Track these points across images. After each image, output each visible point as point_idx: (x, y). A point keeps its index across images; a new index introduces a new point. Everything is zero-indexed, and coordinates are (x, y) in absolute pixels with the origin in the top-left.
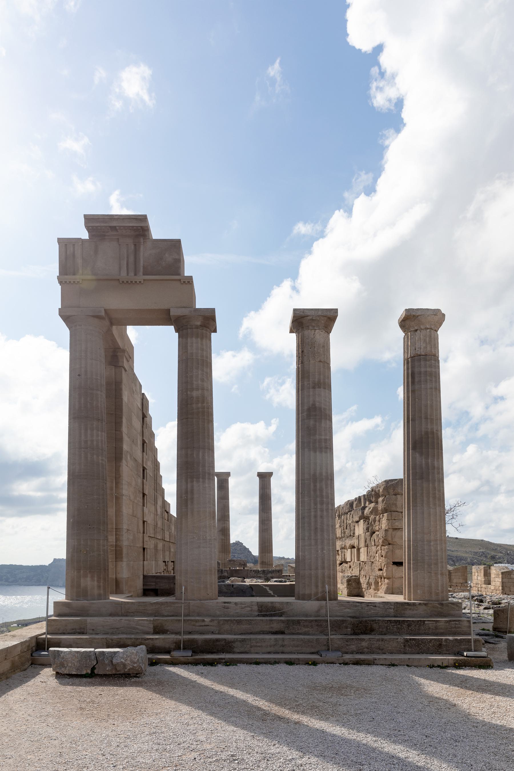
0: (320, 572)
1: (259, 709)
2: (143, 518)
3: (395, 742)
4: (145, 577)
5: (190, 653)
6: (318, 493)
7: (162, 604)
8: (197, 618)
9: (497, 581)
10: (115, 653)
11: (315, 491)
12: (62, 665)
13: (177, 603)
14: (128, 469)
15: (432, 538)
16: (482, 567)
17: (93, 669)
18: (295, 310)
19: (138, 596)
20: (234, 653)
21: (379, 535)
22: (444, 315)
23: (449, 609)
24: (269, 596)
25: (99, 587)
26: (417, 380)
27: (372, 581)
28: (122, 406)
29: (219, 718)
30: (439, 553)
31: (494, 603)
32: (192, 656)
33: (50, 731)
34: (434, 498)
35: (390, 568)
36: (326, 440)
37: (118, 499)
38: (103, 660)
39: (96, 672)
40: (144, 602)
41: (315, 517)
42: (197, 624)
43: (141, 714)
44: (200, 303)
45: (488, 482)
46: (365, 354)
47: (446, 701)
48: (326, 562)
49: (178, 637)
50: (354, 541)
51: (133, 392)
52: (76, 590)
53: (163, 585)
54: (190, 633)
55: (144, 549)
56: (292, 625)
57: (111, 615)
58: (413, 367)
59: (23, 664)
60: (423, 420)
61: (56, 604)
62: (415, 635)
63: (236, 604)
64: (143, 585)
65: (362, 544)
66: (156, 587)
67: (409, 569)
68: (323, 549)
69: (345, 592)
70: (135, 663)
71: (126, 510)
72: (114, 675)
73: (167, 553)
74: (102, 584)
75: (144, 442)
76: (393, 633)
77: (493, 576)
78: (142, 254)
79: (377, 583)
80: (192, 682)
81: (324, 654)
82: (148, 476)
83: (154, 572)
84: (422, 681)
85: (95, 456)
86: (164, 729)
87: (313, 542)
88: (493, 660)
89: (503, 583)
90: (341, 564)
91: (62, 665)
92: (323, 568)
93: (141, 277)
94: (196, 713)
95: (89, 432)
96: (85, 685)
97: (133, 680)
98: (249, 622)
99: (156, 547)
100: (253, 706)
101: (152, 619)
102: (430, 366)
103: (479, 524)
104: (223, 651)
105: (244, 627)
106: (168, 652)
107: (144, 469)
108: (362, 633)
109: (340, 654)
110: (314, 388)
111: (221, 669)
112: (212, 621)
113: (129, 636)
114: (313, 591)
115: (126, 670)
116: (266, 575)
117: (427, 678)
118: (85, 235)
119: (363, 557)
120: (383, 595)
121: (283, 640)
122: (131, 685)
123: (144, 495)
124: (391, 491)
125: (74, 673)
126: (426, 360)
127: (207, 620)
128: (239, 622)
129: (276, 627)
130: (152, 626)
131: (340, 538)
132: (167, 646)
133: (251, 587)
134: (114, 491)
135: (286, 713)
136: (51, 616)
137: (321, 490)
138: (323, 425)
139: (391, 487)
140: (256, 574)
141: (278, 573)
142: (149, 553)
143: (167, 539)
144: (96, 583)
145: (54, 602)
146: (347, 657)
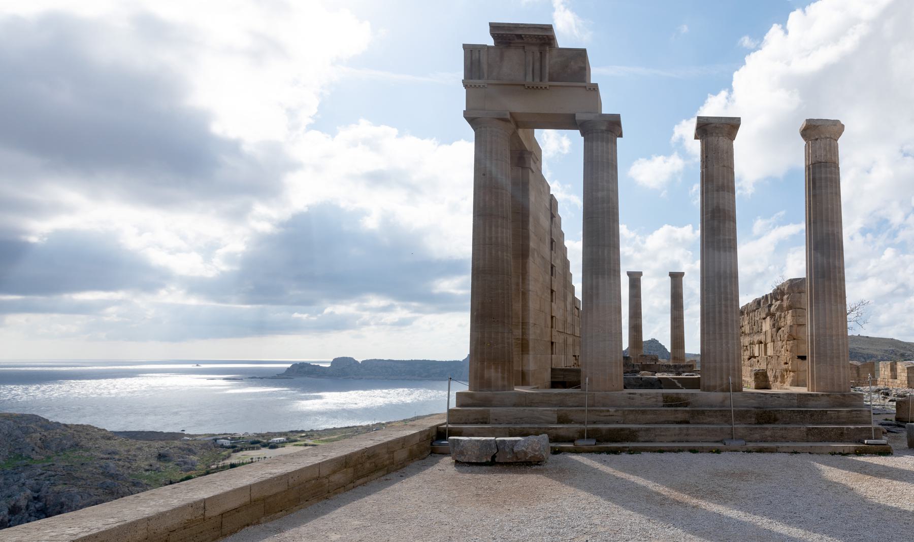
0: (724, 364)
1: (658, 494)
3: (789, 524)
4: (553, 370)
7: (567, 395)
9: (903, 376)
10: (516, 441)
12: (462, 453)
14: (534, 267)
15: (834, 333)
16: (889, 363)
17: (494, 457)
20: (638, 442)
21: (785, 330)
22: (843, 126)
23: (847, 400)
24: (678, 388)
25: (503, 378)
26: (818, 185)
27: (778, 374)
29: (617, 503)
30: (841, 347)
31: (899, 396)
33: (442, 516)
34: (836, 295)
35: (795, 362)
36: (730, 240)
37: (525, 294)
38: (504, 448)
39: (496, 460)
41: (720, 312)
43: (538, 499)
44: (606, 109)
45: (903, 285)
46: (764, 162)
47: (844, 485)
48: (731, 355)
49: (583, 426)
50: (762, 337)
52: (479, 380)
53: (571, 378)
54: (595, 423)
55: (552, 343)
56: (697, 415)
57: (515, 405)
58: (814, 173)
59: (422, 453)
60: (824, 223)
62: (817, 424)
63: (641, 395)
65: (769, 340)
66: (564, 379)
67: (812, 362)
68: (727, 343)
69: (753, 385)
70: (536, 451)
71: (533, 305)
73: (578, 348)
75: (552, 241)
76: (796, 423)
77: (899, 371)
78: (547, 62)
79: (783, 376)
80: (594, 469)
81: (727, 443)
84: (823, 467)
86: (559, 514)
88: (893, 448)
89: (908, 377)
90: (749, 359)
91: (462, 453)
92: (728, 361)
93: (546, 83)
94: (593, 498)
96: (484, 472)
98: (654, 412)
99: (565, 342)
100: (653, 492)
101: (556, 409)
102: (831, 173)
103: (892, 324)
105: (649, 417)
106: (572, 441)
107: (552, 267)
108: (766, 423)
109: (744, 442)
110: (718, 191)
111: (624, 457)
112: (616, 411)
113: (532, 426)
114: (718, 382)
116: (677, 369)
117: (828, 465)
118: (490, 42)
119: (770, 352)
120: (788, 387)
121: (688, 429)
122: (532, 473)
123: (552, 291)
124: (795, 289)
126: (826, 167)
127: (612, 410)
128: (644, 412)
129: (680, 416)
130: (556, 416)
131: (749, 334)
132: (571, 435)
133: (659, 380)
135: (686, 498)
137: (726, 287)
138: (727, 225)
139: (795, 285)
140: (667, 369)
141: (690, 367)
142: (557, 347)
143: (577, 333)
144: (500, 375)
146: (751, 445)
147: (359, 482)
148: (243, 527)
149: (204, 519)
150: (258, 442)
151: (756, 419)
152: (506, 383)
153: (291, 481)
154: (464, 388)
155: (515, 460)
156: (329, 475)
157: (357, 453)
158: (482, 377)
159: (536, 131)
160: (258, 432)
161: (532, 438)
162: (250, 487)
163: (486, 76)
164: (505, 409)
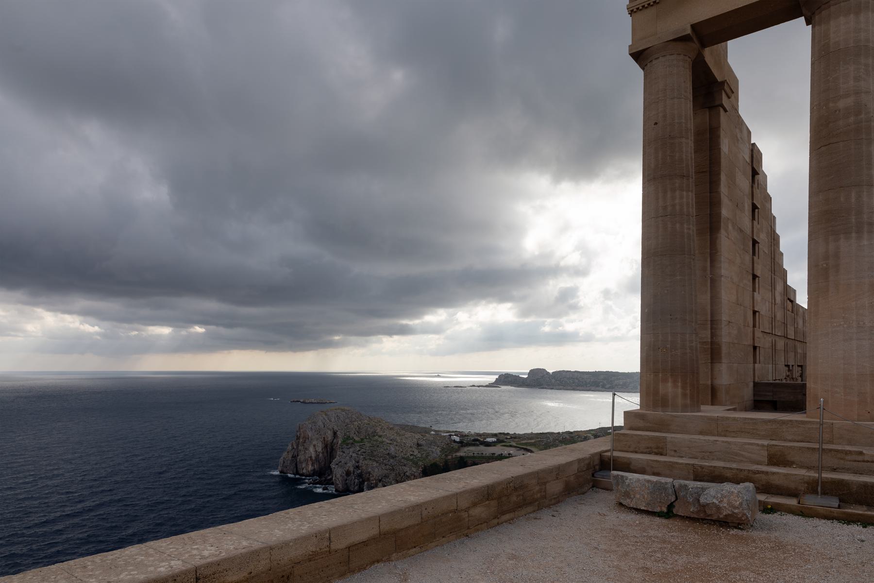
2: (753, 307)
4: (756, 384)
5: (835, 502)
8: (848, 448)
13: (810, 422)
17: (671, 506)
19: (746, 410)
25: (684, 395)
28: (720, 158)
32: (839, 507)
40: (751, 419)
42: (849, 457)
51: (738, 140)
52: (651, 397)
54: (834, 470)
55: (755, 348)
61: (627, 414)
64: (754, 395)
70: (736, 508)
71: (727, 295)
72: (703, 519)
74: (688, 392)
75: (754, 207)
82: (761, 253)
83: (770, 378)
85: (678, 225)
95: (669, 194)
97: (732, 532)
99: (774, 346)
101: (766, 442)
107: (755, 242)
113: (728, 465)
115: (721, 516)
123: (755, 277)
125: (643, 508)
130: (765, 453)
132: (792, 486)
134: (709, 272)
136: (620, 428)
143: (791, 334)
144: (680, 390)
145: (625, 412)
148: (373, 563)
149: (330, 553)
150: (477, 440)
152: (689, 401)
153: (425, 513)
155: (702, 515)
157: (499, 483)
160: (477, 432)
161: (727, 487)
162: (379, 518)
164: (686, 437)
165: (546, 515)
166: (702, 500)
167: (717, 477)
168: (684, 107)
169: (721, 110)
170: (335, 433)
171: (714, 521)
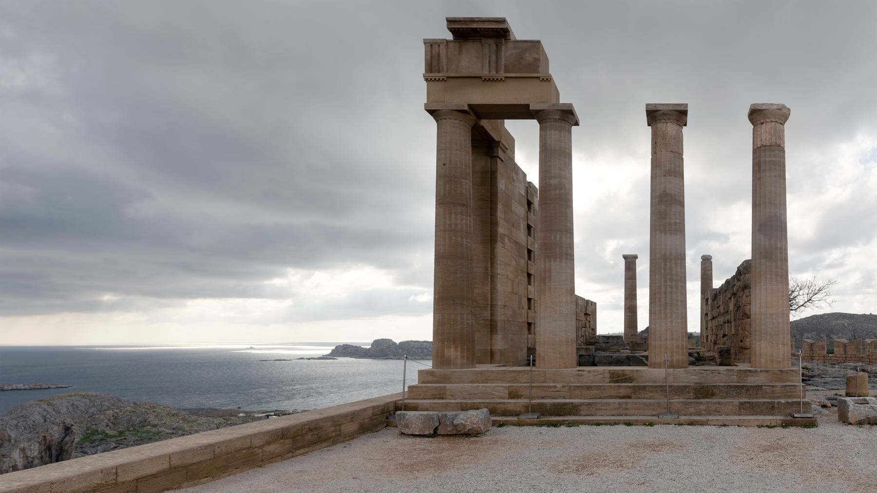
6: (668, 271)
7: (520, 372)
11: (665, 270)
12: (406, 426)
17: (436, 429)
18: (647, 105)
22: (789, 110)
25: (462, 357)
26: (762, 168)
41: (665, 293)
51: (514, 181)
52: (441, 360)
54: (543, 398)
63: (589, 371)
71: (503, 288)
78: (503, 54)
87: (663, 316)
91: (406, 426)
95: (453, 216)
98: (599, 388)
104: (570, 414)
106: (517, 414)
112: (563, 387)
118: (449, 36)
121: (627, 403)
129: (623, 392)
130: (507, 392)
132: (518, 409)
137: (671, 269)
144: (459, 353)
147: (298, 452)
151: (695, 394)
152: (465, 361)
154: (428, 365)
155: (455, 432)
156: (263, 446)
157: (294, 426)
158: (443, 356)
159: (506, 121)
162: (170, 456)
163: (445, 69)
164: (460, 385)
165: (338, 447)
166: (455, 422)
167: (464, 408)
168: (465, 156)
169: (499, 160)
170: (67, 429)
171: (462, 435)
